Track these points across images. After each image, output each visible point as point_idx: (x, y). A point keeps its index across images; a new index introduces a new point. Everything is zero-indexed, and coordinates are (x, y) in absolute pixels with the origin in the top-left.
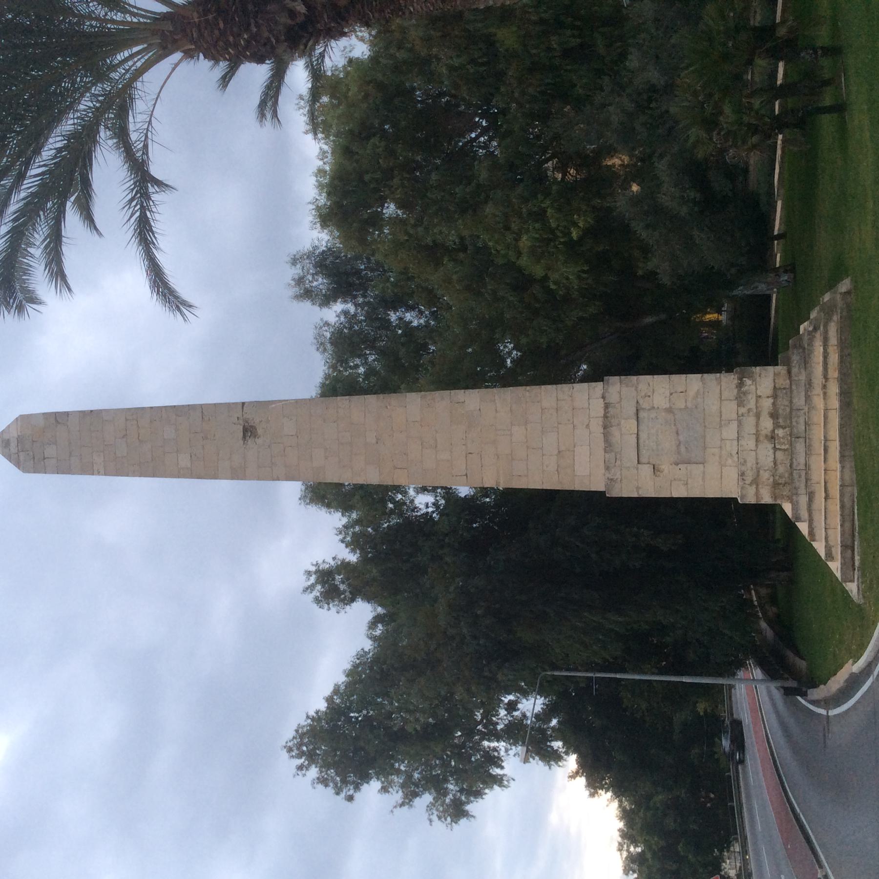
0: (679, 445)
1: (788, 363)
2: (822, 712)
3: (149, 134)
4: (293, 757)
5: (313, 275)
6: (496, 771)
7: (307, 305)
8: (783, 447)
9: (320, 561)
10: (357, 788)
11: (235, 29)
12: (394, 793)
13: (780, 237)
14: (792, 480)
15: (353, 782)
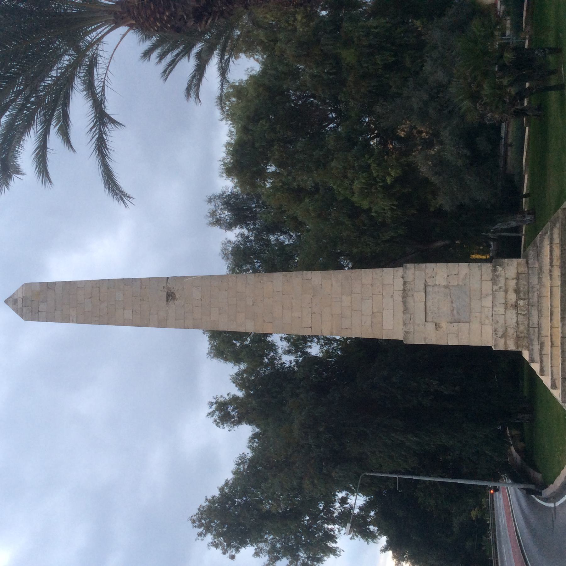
0: (452, 311)
1: (526, 257)
2: (552, 505)
3: (106, 81)
4: (195, 526)
5: (221, 209)
6: (331, 545)
7: (217, 229)
8: (523, 313)
9: (219, 396)
10: (237, 550)
11: (161, 9)
12: (263, 556)
13: (526, 196)
14: (529, 334)
15: (235, 547)
